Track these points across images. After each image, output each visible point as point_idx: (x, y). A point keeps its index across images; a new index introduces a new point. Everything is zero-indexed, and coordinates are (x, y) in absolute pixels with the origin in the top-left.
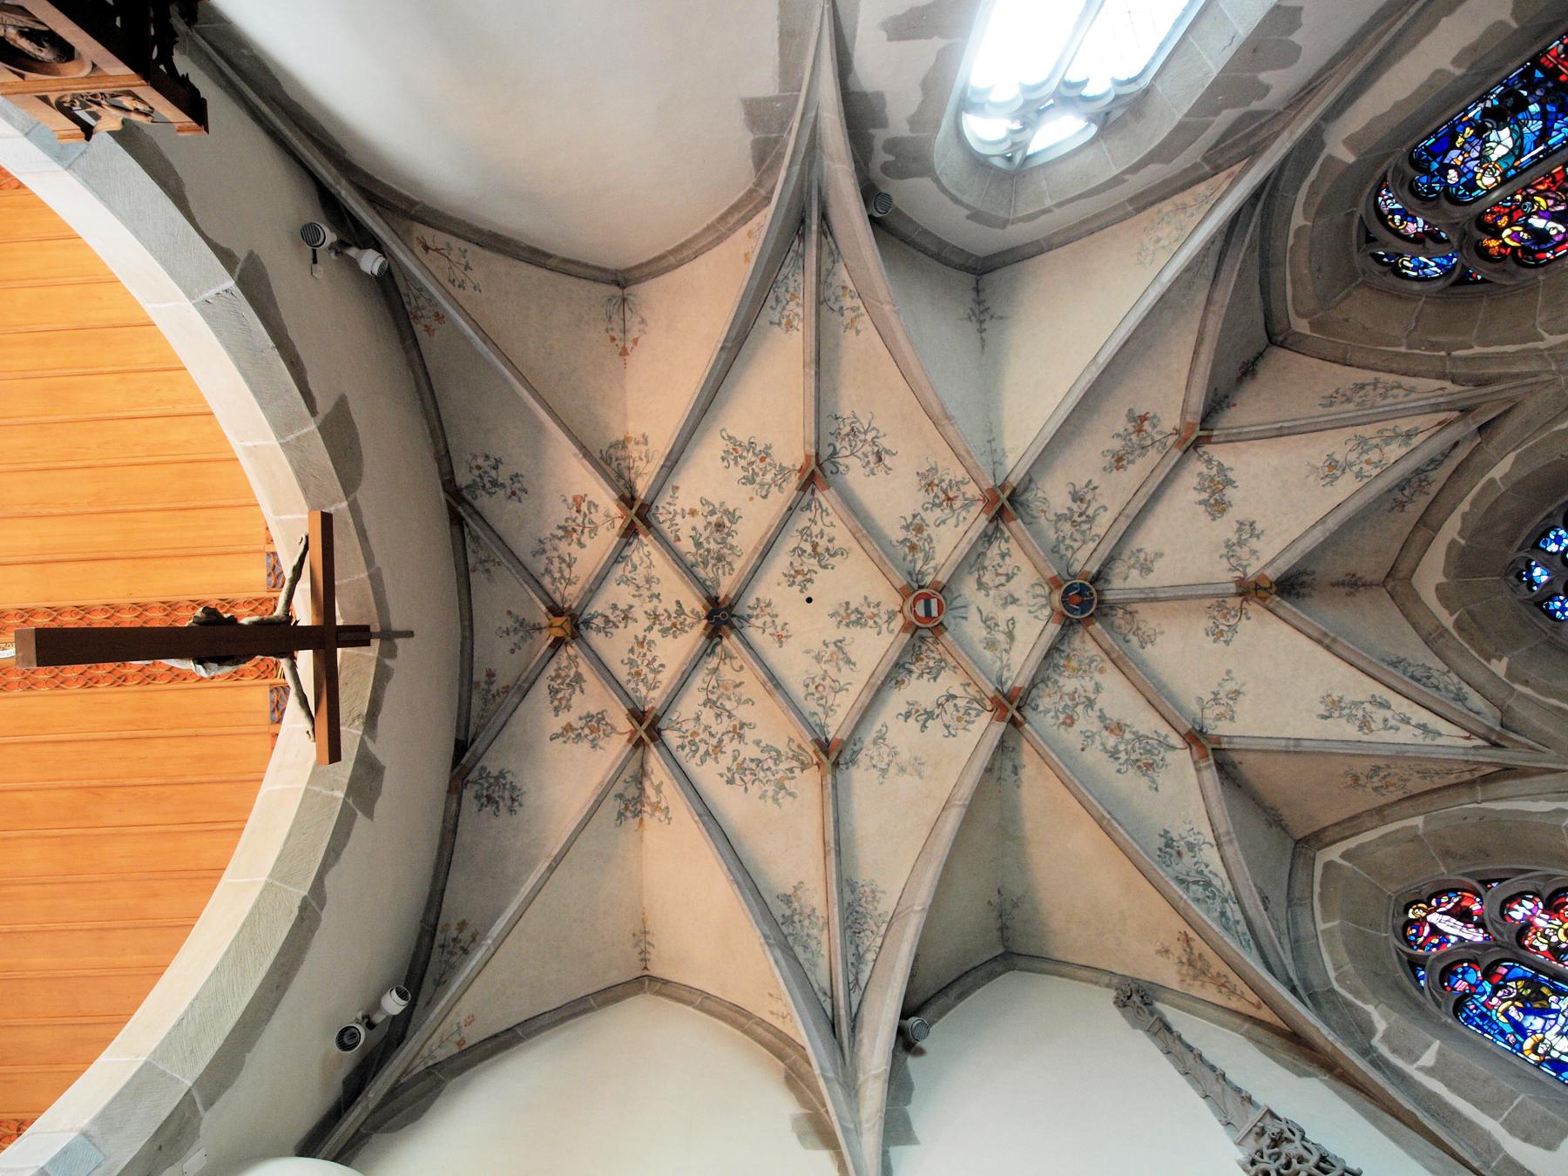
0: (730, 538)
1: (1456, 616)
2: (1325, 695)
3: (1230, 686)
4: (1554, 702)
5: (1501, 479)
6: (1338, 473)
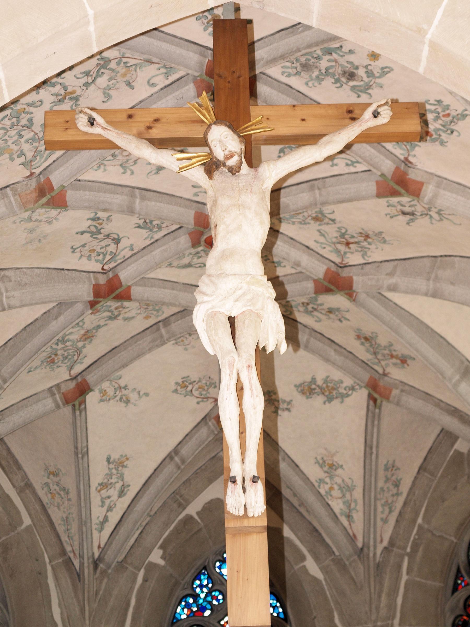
0: (333, 80)
1: (196, 517)
2: (128, 457)
3: (133, 397)
4: (133, 602)
5: (304, 566)
6: (326, 468)
